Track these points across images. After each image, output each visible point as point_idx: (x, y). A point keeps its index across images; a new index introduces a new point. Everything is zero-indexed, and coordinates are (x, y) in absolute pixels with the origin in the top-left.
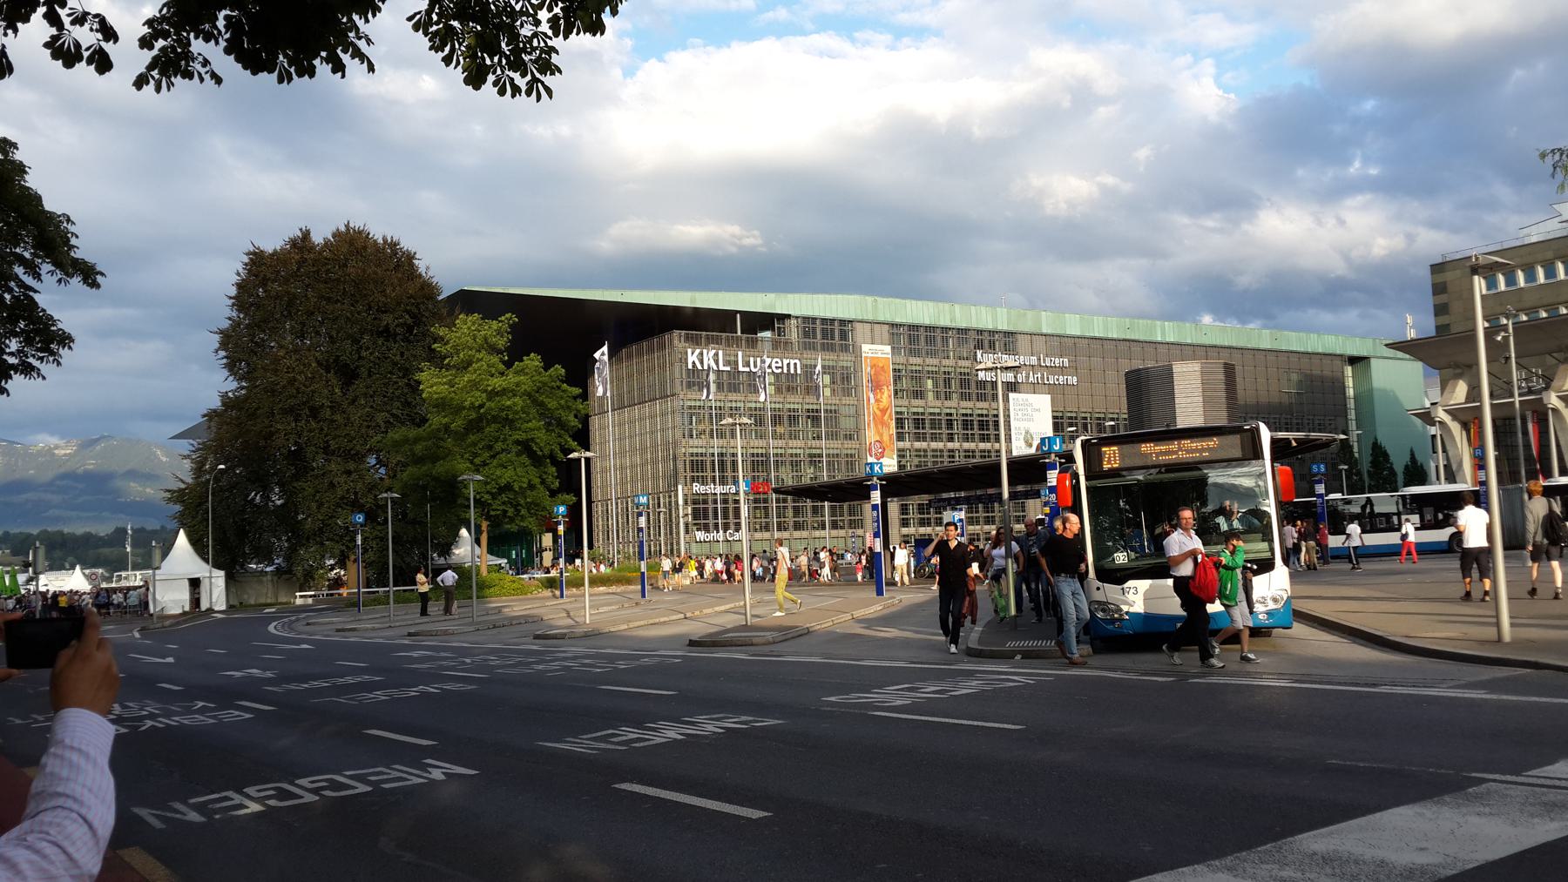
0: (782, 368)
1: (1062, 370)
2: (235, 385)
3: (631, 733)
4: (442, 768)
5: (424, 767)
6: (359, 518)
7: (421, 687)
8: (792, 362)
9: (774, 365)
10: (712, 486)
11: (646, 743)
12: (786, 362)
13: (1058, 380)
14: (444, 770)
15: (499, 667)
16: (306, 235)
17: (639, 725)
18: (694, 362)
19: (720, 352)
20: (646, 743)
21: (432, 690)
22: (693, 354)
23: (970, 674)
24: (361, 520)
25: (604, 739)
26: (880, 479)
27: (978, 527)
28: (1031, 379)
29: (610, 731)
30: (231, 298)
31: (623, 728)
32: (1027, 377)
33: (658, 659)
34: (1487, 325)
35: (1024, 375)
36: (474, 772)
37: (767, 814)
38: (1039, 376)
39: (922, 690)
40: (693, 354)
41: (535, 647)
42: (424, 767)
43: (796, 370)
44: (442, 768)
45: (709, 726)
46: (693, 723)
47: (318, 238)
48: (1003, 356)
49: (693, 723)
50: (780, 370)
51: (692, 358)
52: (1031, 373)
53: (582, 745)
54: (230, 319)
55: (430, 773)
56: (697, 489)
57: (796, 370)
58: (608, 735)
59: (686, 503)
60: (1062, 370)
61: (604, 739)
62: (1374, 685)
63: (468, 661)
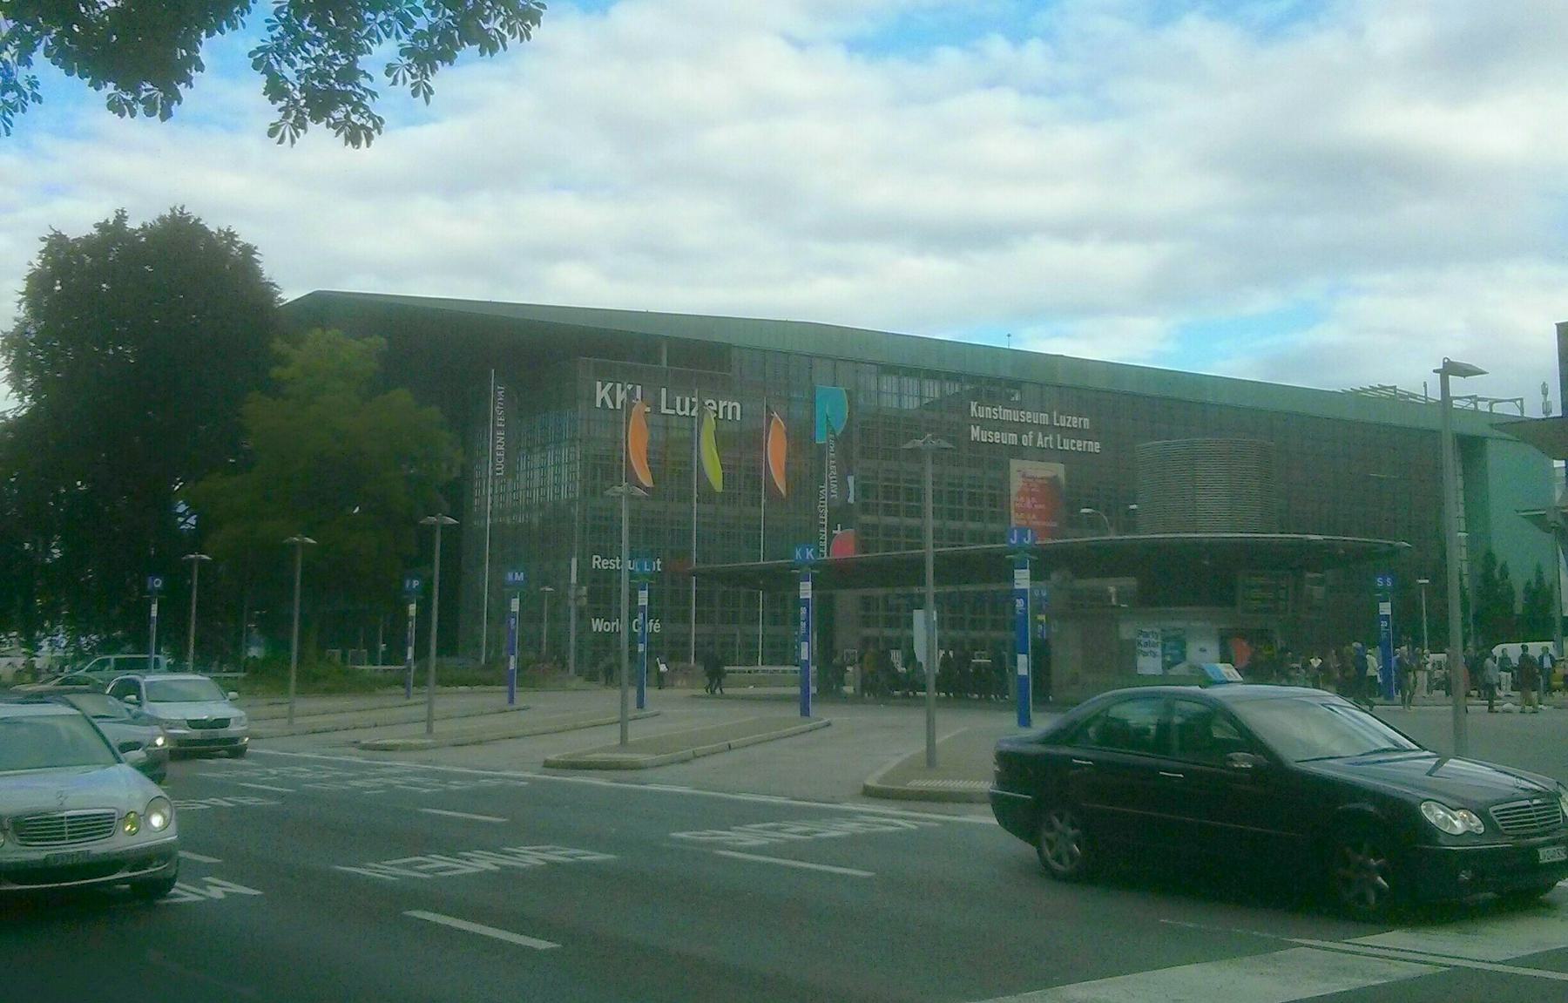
1: (1078, 433)
2: (15, 403)
3: (438, 861)
4: (222, 886)
5: (204, 886)
6: (157, 583)
7: (213, 799)
8: (730, 405)
10: (618, 561)
11: (455, 873)
12: (722, 404)
13: (1075, 445)
14: (224, 889)
15: (306, 781)
16: (121, 217)
17: (451, 852)
18: (603, 400)
20: (455, 873)
21: (224, 804)
22: (603, 388)
23: (848, 815)
24: (159, 586)
25: (408, 866)
26: (812, 567)
27: (982, 634)
28: (1040, 443)
29: (419, 858)
30: (21, 293)
31: (433, 856)
32: (1035, 440)
33: (499, 782)
34: (409, 674)
35: (1031, 437)
36: (257, 892)
37: (553, 946)
38: (1051, 438)
39: (787, 830)
40: (603, 388)
41: (360, 760)
42: (204, 886)
43: (734, 414)
44: (222, 886)
45: (530, 857)
46: (513, 854)
47: (133, 224)
48: (1005, 410)
49: (513, 854)
51: (602, 393)
52: (1040, 435)
53: (387, 871)
54: (16, 319)
55: (209, 891)
56: (598, 563)
57: (734, 414)
58: (412, 863)
59: (580, 582)
60: (1078, 433)
61: (408, 866)
62: (498, 771)
63: (274, 772)
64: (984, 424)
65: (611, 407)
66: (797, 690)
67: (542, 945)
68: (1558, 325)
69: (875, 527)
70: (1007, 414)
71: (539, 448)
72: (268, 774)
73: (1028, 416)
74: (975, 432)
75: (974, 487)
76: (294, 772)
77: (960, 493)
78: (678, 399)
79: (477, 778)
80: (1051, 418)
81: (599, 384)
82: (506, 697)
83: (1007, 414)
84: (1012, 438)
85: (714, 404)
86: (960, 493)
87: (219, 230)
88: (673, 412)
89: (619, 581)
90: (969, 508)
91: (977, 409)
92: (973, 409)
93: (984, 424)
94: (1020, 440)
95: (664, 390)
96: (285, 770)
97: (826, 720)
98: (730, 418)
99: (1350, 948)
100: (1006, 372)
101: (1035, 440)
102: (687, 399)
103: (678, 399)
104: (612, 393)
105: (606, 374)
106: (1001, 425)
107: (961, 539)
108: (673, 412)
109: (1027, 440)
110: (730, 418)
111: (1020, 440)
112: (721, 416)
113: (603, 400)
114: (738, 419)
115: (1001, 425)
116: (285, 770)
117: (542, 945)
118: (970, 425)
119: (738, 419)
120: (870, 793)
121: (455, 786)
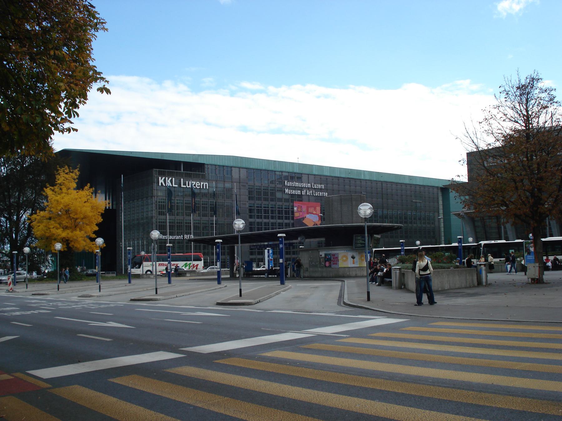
0: (200, 186)
1: (321, 190)
9: (197, 185)
12: (202, 183)
13: (319, 194)
18: (162, 183)
19: (174, 179)
32: (306, 193)
43: (206, 187)
50: (199, 187)
51: (161, 181)
57: (206, 187)
60: (321, 190)
63: (51, 304)
64: (289, 188)
65: (164, 185)
66: (216, 277)
67: (108, 340)
68: (467, 153)
69: (261, 223)
70: (297, 184)
71: (145, 199)
72: (50, 305)
73: (304, 185)
74: (287, 191)
75: (280, 208)
76: (57, 304)
77: (282, 211)
78: (187, 182)
79: (109, 304)
80: (311, 185)
81: (160, 178)
82: (127, 282)
83: (297, 184)
84: (299, 192)
85: (199, 183)
86: (282, 211)
87: (98, 31)
88: (185, 186)
89: (320, 241)
90: (285, 215)
91: (287, 183)
92: (286, 183)
93: (289, 188)
94: (301, 193)
95: (182, 179)
96: (55, 303)
97: (225, 285)
98: (205, 188)
99: (302, 332)
100: (296, 170)
101: (306, 193)
102: (190, 182)
103: (187, 182)
104: (165, 181)
105: (162, 174)
106: (295, 188)
107: (289, 226)
108: (185, 186)
109: (304, 193)
110: (205, 188)
111: (301, 193)
112: (202, 187)
113: (162, 183)
114: (207, 188)
115: (295, 188)
116: (55, 303)
117: (108, 340)
118: (285, 188)
119: (207, 188)
120: (219, 304)
121: (102, 306)
